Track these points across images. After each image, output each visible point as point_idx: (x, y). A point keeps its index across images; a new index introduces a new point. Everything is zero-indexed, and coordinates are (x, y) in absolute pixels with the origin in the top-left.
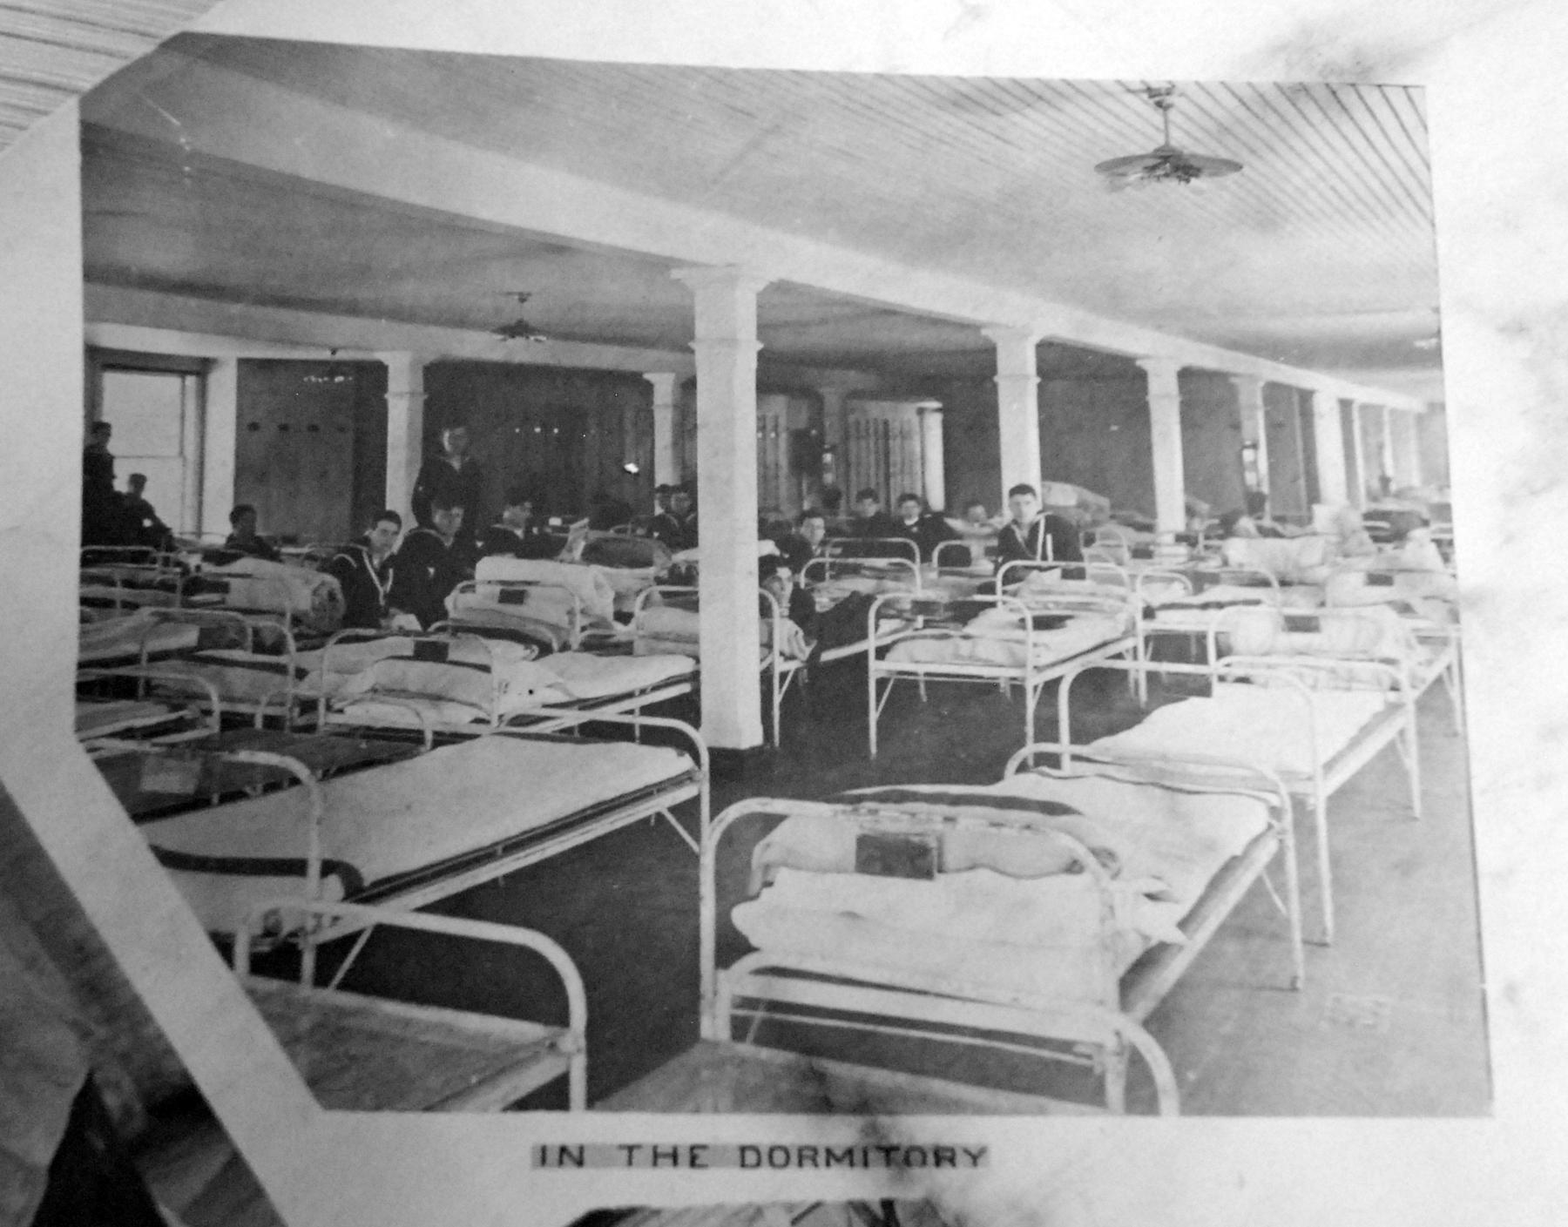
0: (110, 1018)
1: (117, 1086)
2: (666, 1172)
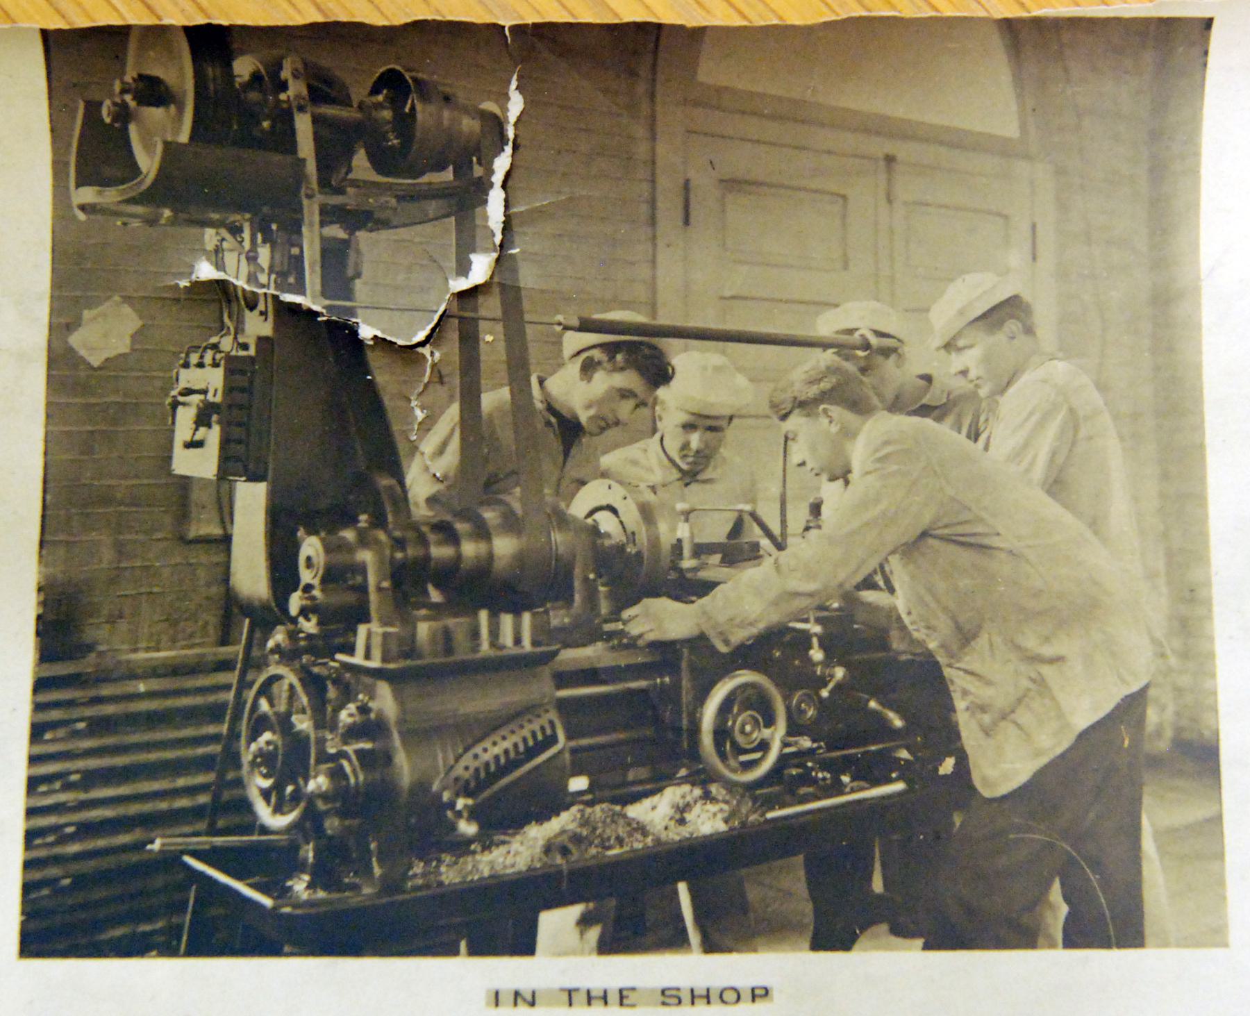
0: (1185, 655)
1: (1163, 709)
2: (701, 984)
